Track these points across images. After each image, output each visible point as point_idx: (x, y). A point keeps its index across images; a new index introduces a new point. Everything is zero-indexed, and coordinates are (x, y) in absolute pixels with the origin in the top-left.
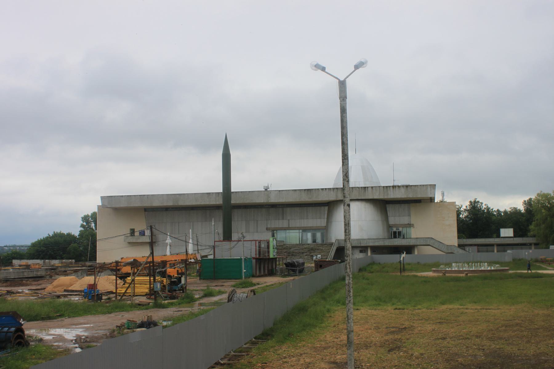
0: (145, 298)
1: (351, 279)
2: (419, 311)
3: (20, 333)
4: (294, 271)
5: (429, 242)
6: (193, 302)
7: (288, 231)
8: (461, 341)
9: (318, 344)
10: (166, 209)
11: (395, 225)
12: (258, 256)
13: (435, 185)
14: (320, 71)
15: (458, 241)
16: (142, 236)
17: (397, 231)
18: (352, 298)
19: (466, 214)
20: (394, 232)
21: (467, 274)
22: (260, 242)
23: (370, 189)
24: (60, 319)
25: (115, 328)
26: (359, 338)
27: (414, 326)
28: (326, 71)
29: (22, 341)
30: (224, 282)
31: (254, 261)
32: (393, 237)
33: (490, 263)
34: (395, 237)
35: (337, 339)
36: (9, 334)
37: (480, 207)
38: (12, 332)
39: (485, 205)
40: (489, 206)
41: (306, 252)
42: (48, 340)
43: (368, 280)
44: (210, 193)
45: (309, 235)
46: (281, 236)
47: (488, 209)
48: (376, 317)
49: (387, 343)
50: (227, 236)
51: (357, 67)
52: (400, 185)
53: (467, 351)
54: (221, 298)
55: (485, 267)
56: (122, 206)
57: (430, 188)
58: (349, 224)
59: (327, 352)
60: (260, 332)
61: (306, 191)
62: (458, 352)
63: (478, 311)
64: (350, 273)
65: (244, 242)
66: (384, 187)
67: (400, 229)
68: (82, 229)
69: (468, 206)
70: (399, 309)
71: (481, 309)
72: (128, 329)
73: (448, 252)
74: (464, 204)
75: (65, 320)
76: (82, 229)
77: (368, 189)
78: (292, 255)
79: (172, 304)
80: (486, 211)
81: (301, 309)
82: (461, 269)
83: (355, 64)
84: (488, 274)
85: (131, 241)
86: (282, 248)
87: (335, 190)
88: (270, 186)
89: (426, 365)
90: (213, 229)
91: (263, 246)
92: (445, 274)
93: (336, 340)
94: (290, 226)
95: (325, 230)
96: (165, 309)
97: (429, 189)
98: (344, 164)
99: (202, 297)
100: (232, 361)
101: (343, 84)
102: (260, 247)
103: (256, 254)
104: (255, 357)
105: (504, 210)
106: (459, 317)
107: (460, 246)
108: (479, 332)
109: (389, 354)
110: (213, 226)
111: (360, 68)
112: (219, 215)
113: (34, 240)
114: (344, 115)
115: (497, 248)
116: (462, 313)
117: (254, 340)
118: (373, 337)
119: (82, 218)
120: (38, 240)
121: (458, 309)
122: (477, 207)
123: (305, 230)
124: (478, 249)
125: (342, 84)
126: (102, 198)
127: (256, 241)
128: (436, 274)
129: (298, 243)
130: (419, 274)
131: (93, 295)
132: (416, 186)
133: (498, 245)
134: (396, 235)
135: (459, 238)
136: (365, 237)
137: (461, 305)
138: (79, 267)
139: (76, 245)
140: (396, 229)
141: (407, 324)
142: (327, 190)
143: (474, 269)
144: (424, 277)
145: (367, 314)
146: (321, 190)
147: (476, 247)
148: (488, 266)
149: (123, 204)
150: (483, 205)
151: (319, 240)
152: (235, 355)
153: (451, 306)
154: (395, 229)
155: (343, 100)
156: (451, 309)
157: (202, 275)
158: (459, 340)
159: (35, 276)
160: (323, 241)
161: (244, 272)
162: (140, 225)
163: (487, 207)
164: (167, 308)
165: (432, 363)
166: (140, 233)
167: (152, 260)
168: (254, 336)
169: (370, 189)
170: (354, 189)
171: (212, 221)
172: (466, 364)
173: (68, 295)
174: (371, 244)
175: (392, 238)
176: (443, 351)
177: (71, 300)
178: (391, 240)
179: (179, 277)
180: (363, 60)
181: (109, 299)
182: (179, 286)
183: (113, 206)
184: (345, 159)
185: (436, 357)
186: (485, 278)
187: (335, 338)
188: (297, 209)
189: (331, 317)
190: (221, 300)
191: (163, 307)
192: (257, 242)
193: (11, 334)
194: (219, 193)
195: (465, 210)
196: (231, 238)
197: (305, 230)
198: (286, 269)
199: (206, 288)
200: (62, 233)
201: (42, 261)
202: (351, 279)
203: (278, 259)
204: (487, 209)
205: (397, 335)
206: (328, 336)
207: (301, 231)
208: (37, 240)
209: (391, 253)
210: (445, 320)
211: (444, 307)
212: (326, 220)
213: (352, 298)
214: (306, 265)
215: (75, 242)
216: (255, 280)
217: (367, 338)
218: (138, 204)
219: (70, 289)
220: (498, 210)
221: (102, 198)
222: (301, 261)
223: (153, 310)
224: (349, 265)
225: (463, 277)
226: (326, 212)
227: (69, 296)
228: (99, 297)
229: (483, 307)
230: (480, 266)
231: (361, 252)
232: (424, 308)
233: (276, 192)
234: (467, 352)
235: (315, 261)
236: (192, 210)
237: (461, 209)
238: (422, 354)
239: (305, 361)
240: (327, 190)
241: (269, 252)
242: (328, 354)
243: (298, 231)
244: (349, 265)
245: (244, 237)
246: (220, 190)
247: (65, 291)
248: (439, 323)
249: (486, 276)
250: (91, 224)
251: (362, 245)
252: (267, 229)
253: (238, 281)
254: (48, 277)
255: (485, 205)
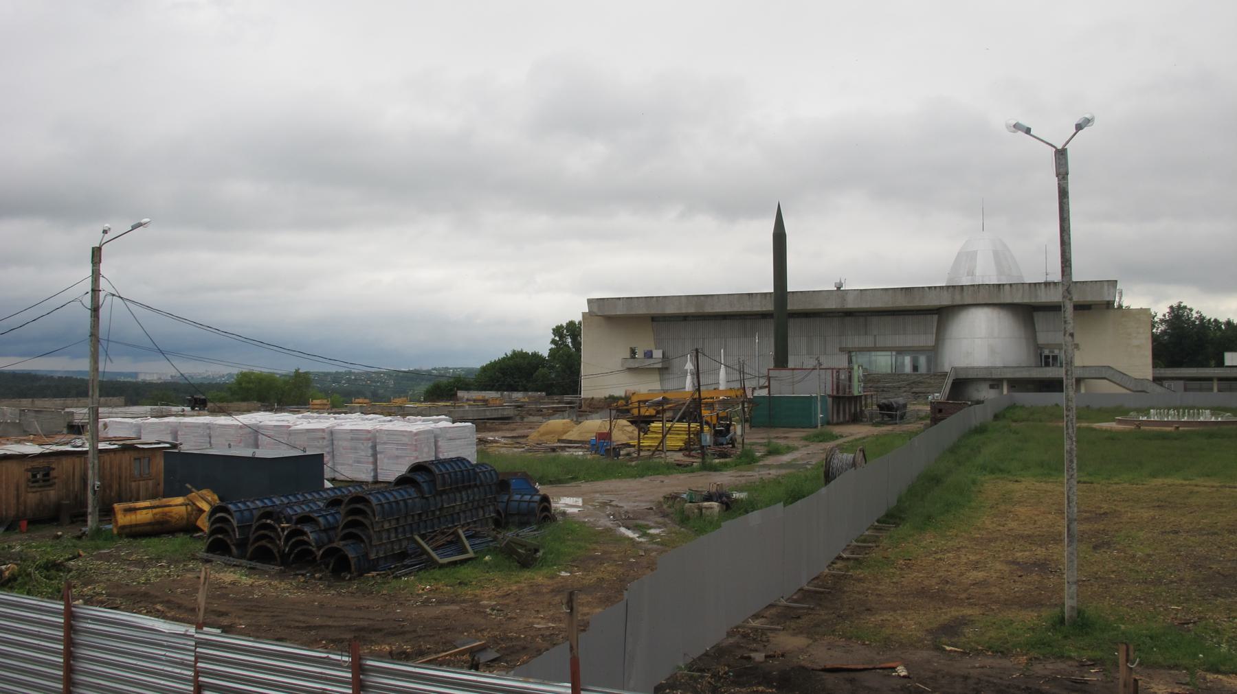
0: (681, 454)
1: (1074, 443)
2: (1118, 486)
3: (546, 504)
4: (890, 416)
5: (1105, 373)
6: (754, 462)
7: (873, 353)
8: (1205, 537)
9: (976, 534)
10: (685, 318)
11: (1047, 346)
12: (835, 393)
13: (1116, 281)
14: (1021, 134)
15: (1153, 371)
16: (648, 358)
17: (1051, 355)
18: (1075, 471)
19: (1162, 327)
20: (1045, 356)
21: (1178, 428)
22: (838, 372)
23: (1007, 288)
24: (573, 484)
25: (662, 500)
26: (1038, 526)
27: (1119, 511)
28: (1032, 133)
29: (549, 514)
30: (787, 433)
31: (830, 400)
32: (1043, 365)
33: (1215, 410)
34: (1047, 364)
35: (1003, 526)
36: (532, 504)
37: (1188, 315)
38: (536, 502)
39: (1197, 313)
40: (1204, 315)
41: (904, 387)
42: (573, 513)
43: (1018, 433)
44: (752, 294)
45: (907, 360)
46: (861, 359)
47: (1202, 318)
48: (1050, 494)
49: (1086, 536)
50: (781, 361)
51: (1079, 127)
52: (1056, 281)
53: (1222, 553)
54: (795, 457)
55: (1206, 416)
56: (618, 313)
57: (1108, 286)
58: (1071, 362)
59: (999, 547)
60: (883, 513)
61: (904, 291)
62: (1208, 554)
63: (1217, 490)
64: (1073, 435)
65: (821, 371)
66: (1030, 284)
67: (1056, 352)
68: (553, 346)
69: (1167, 314)
70: (1085, 483)
71: (1221, 487)
72: (690, 502)
73: (1135, 390)
74: (1161, 310)
75: (583, 485)
76: (553, 346)
77: (1003, 289)
78: (883, 391)
79: (725, 465)
80: (1197, 323)
81: (932, 480)
82: (1166, 419)
83: (1076, 123)
84: (1215, 428)
85: (633, 366)
86: (870, 379)
87: (950, 290)
88: (843, 282)
89: (1162, 573)
90: (757, 349)
91: (843, 377)
92: (1140, 427)
93: (1001, 528)
94: (877, 346)
95: (934, 352)
96: (718, 473)
97: (1106, 287)
98: (1065, 274)
99: (764, 455)
100: (857, 554)
101: (1062, 154)
102: (838, 378)
103: (833, 390)
104: (889, 550)
105: (1226, 320)
106: (1187, 498)
107: (1157, 380)
108: (1231, 523)
109: (1096, 553)
110: (757, 345)
111: (1085, 128)
112: (770, 327)
113: (485, 363)
114: (1065, 200)
115: (1218, 384)
116: (1191, 493)
117: (876, 524)
118: (1059, 526)
119: (554, 330)
120: (491, 363)
121: (1182, 485)
122: (1183, 316)
123: (901, 351)
124: (1185, 385)
125: (1061, 154)
126: (590, 301)
127: (832, 369)
128: (1121, 427)
129: (889, 372)
130: (1096, 425)
131: (608, 449)
132: (1083, 282)
133: (1220, 379)
134: (1048, 361)
135: (1155, 366)
136: (999, 364)
137: (1185, 480)
138: (553, 403)
139: (545, 370)
140: (1050, 352)
141: (1105, 507)
142: (938, 289)
143: (1185, 419)
144: (1106, 431)
145: (1035, 490)
146: (927, 289)
147: (1182, 382)
148: (1212, 415)
149: (620, 311)
150: (1193, 312)
151: (923, 368)
152: (858, 546)
153: (1169, 481)
154: (1046, 352)
155: (1063, 178)
156: (1169, 486)
157: (751, 421)
158: (1203, 535)
159: (500, 416)
160: (929, 369)
161: (821, 418)
162: (644, 343)
163: (1201, 316)
164: (721, 470)
165: (1170, 570)
166: (645, 354)
167: (698, 397)
168: (876, 519)
169: (1007, 288)
170: (981, 287)
171: (755, 338)
172: (1227, 574)
173: (565, 447)
174: (1009, 376)
175: (1041, 366)
176: (1181, 551)
177: (572, 454)
178: (1038, 369)
179: (727, 424)
180: (1088, 116)
181: (628, 454)
182: (727, 437)
183: (606, 313)
184: (1066, 266)
185: (1173, 560)
186: (1211, 435)
187: (999, 525)
188: (889, 319)
189: (980, 492)
190: (794, 460)
191: (715, 469)
192: (835, 371)
193: (536, 505)
194: (766, 294)
195: (1162, 321)
196: (787, 362)
197: (901, 351)
198: (880, 413)
199: (765, 441)
200: (524, 351)
201: (499, 393)
202: (1074, 443)
203: (863, 398)
204: (1201, 319)
205: (1096, 523)
206: (986, 522)
207: (894, 353)
208: (489, 363)
209: (1040, 391)
210: (1165, 502)
211: (1159, 481)
212: (934, 336)
213: (1075, 471)
214: (910, 408)
215: (543, 367)
216: (837, 430)
217: (1050, 527)
218: (642, 310)
219: (564, 437)
220: (1216, 320)
221: (590, 301)
222: (901, 400)
223: (701, 473)
224: (1072, 423)
225: (1171, 432)
226: (935, 324)
227: (568, 449)
228: (615, 452)
229: (1222, 484)
230: (1199, 414)
231: (992, 387)
232: (1125, 482)
233: (856, 292)
234: (1223, 556)
235: (931, 402)
236: (724, 319)
237: (1155, 318)
238: (1149, 555)
239: (968, 558)
240: (938, 289)
241: (850, 387)
242: (1000, 549)
243: (889, 353)
244: (1072, 423)
245: (820, 364)
246: (770, 289)
247: (559, 441)
248: (1158, 506)
249: (1211, 432)
250: (566, 339)
251: (994, 377)
252: (842, 350)
253: (811, 431)
254: (518, 418)
255: (1197, 313)
